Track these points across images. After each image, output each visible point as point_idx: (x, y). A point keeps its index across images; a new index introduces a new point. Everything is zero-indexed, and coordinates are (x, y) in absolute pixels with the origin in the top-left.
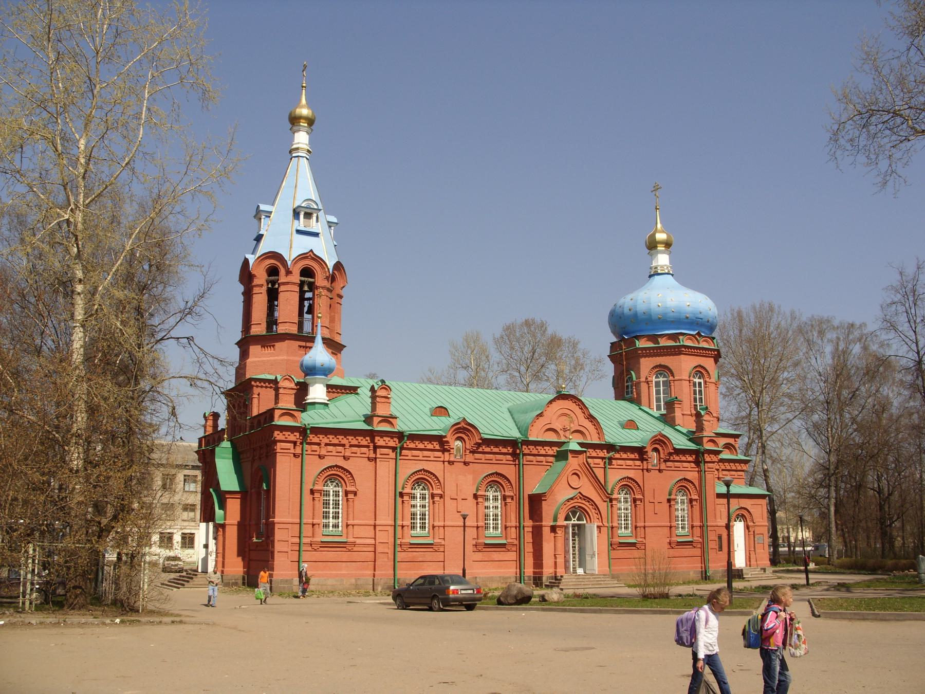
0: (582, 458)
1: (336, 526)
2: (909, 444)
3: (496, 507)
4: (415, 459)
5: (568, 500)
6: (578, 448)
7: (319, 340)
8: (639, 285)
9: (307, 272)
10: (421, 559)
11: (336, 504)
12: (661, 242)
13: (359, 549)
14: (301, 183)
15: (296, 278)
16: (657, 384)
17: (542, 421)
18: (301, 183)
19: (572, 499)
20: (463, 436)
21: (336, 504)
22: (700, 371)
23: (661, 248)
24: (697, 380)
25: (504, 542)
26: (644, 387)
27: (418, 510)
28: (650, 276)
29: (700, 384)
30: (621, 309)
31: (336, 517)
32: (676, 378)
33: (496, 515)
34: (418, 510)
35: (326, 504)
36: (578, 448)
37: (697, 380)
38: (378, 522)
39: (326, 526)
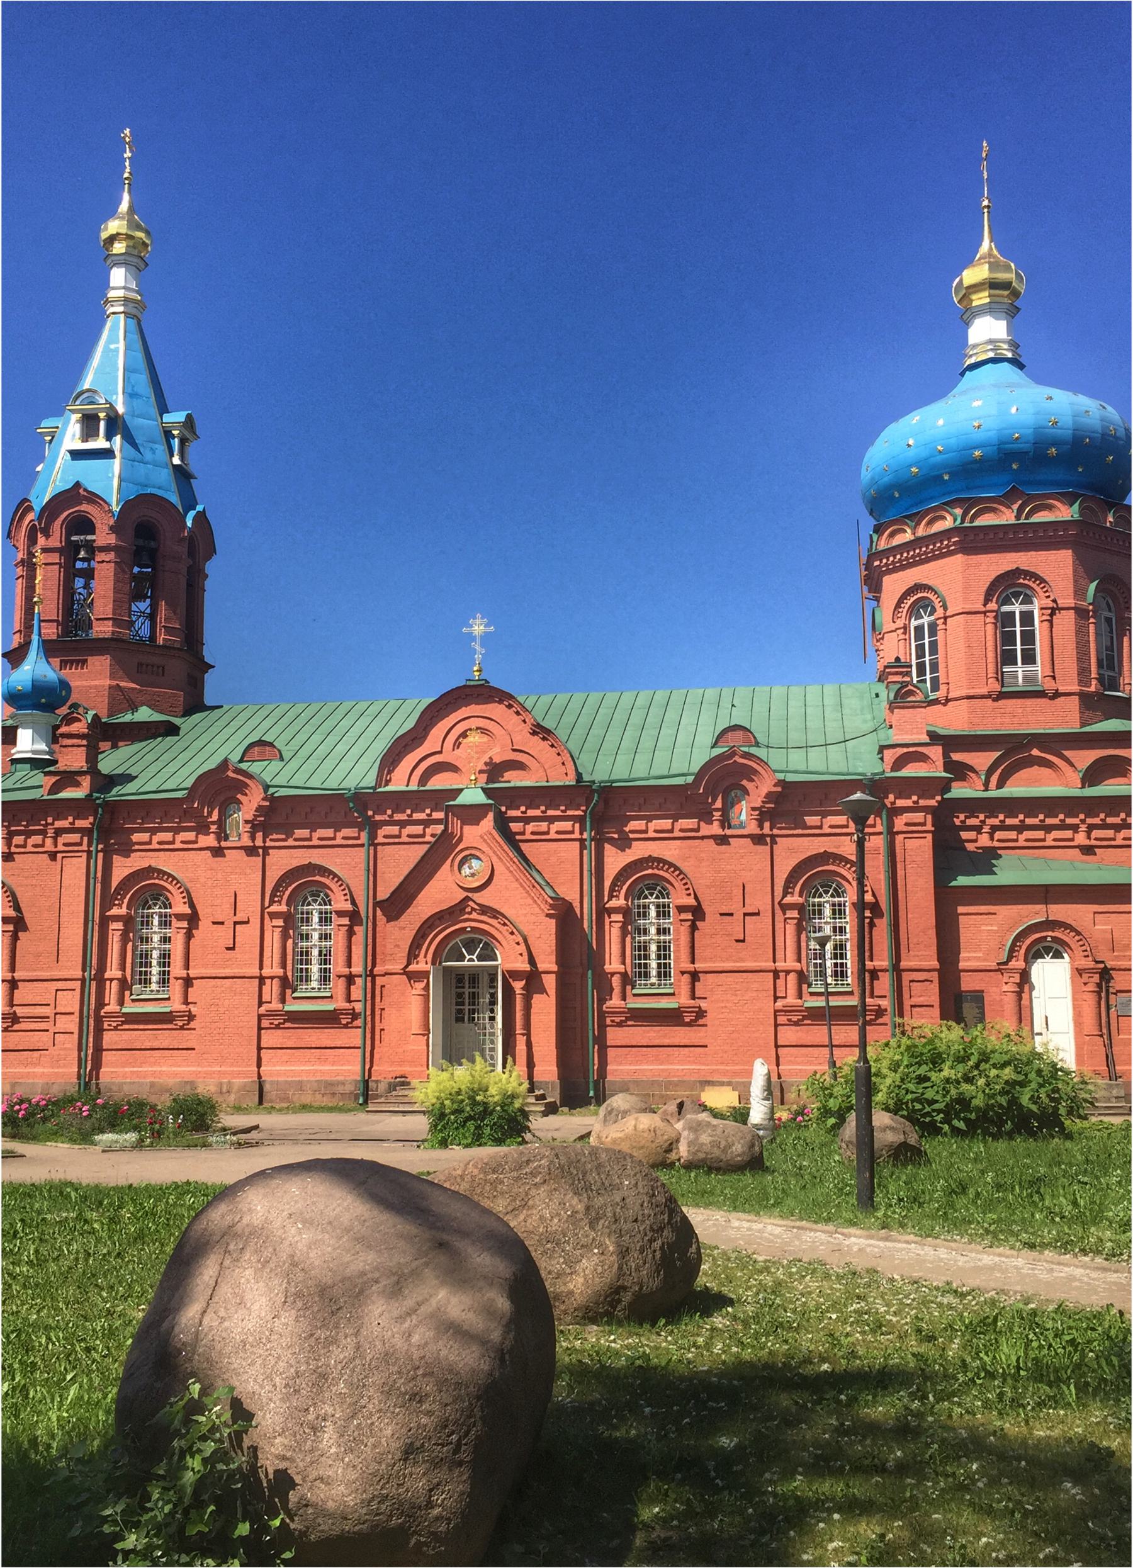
29: (1027, 618)
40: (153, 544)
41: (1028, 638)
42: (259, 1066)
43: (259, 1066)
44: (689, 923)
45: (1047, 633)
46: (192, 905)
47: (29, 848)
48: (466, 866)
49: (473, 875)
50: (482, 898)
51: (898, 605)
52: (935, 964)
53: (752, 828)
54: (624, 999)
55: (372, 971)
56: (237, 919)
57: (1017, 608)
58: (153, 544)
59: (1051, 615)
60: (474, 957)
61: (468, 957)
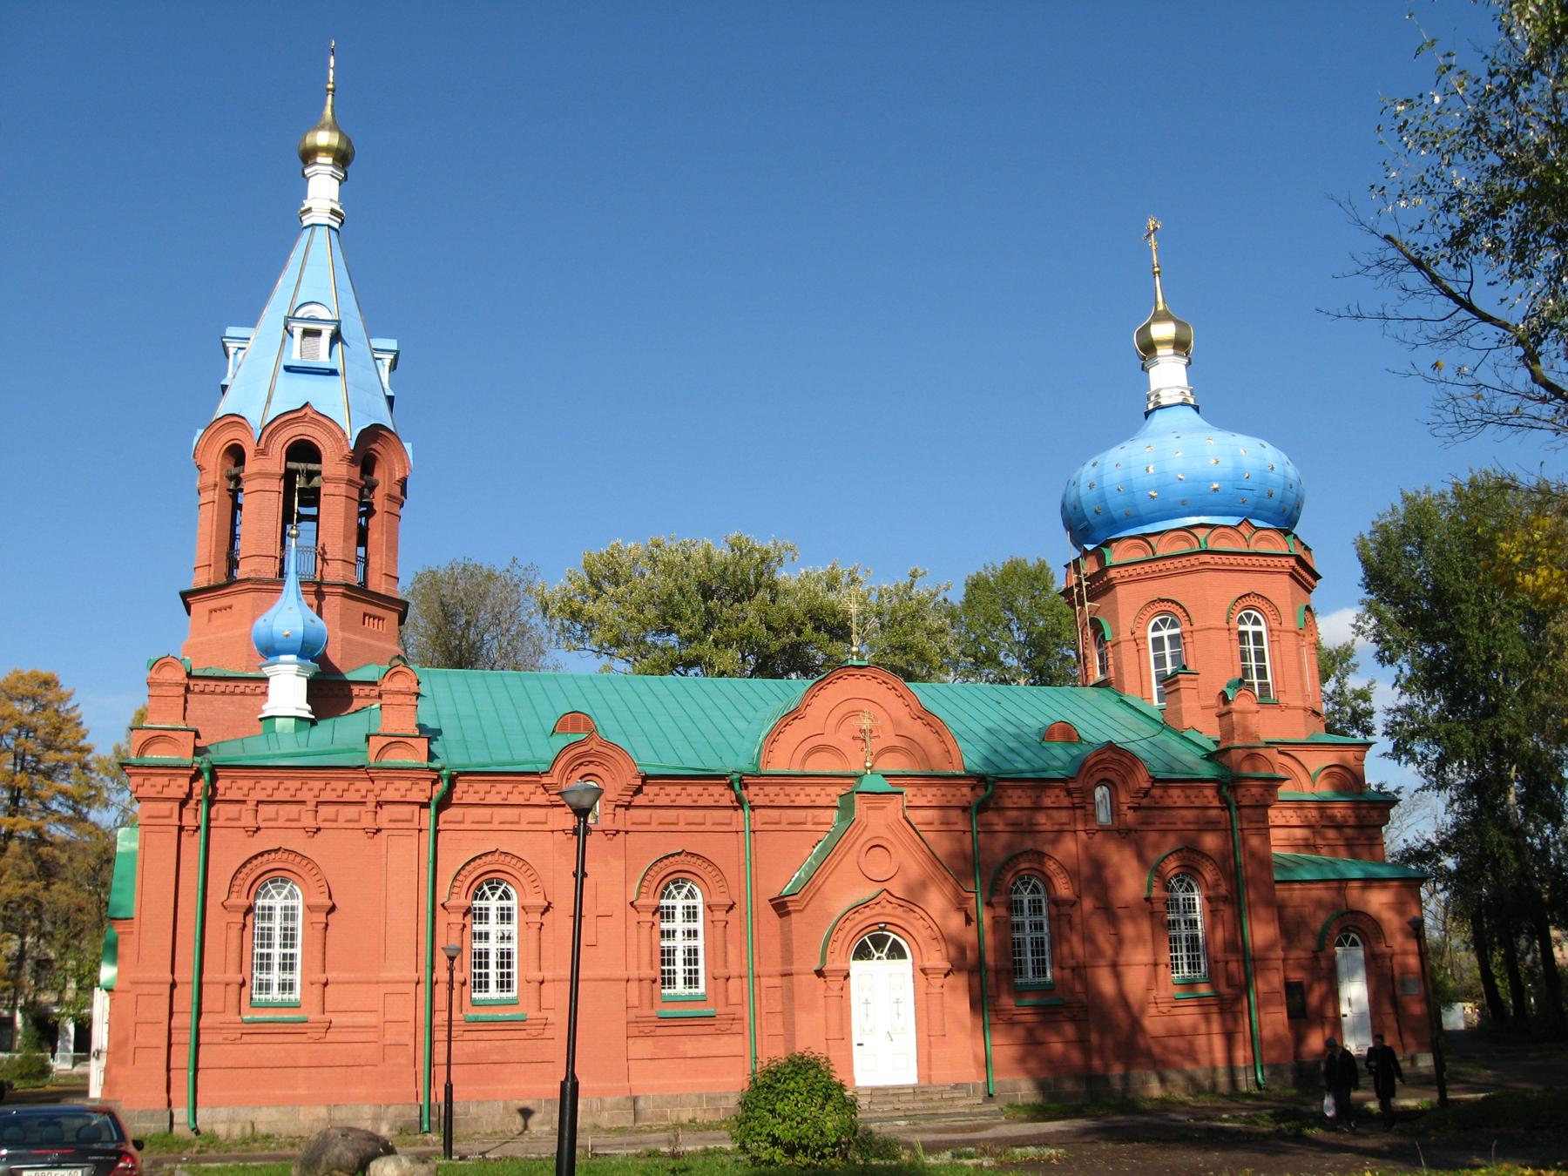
0: (894, 807)
1: (286, 986)
2: (643, 575)
3: (692, 934)
4: (483, 827)
5: (855, 909)
6: (885, 785)
7: (292, 581)
8: (1128, 432)
9: (304, 451)
10: (496, 1058)
11: (288, 938)
12: (1164, 343)
13: (340, 1038)
14: (315, 278)
15: (276, 462)
16: (1158, 643)
17: (796, 732)
18: (315, 278)
19: (865, 904)
20: (591, 769)
21: (288, 938)
22: (1249, 602)
23: (1164, 352)
24: (1249, 628)
25: (709, 1011)
26: (1127, 651)
27: (493, 946)
28: (1147, 414)
29: (1258, 637)
30: (1094, 492)
31: (287, 965)
32: (1196, 626)
33: (693, 952)
34: (493, 946)
35: (266, 936)
36: (885, 785)
37: (1249, 628)
38: (331, 975)
39: (265, 987)
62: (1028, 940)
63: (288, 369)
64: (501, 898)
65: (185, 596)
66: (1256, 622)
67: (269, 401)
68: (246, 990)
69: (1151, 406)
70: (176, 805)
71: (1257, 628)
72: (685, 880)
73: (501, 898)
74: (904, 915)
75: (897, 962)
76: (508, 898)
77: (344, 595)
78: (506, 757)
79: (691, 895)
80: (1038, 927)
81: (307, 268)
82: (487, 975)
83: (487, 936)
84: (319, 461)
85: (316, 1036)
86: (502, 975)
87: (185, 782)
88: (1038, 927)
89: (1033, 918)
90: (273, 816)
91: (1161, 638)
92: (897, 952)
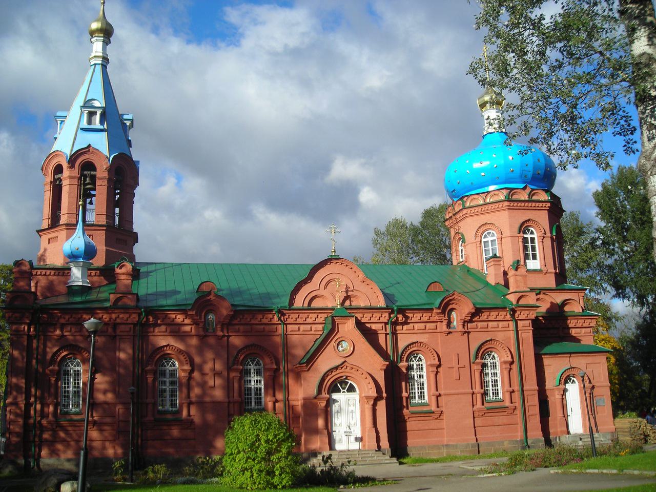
28: (483, 137)
29: (533, 240)
37: (529, 236)
38: (442, 392)
40: (93, 173)
41: (533, 248)
42: (476, 435)
43: (476, 435)
44: (238, 377)
45: (541, 247)
46: (439, 360)
47: (489, 329)
48: (340, 346)
49: (343, 350)
50: (350, 360)
51: (478, 230)
52: (537, 388)
53: (460, 328)
54: (483, 404)
55: (288, 399)
56: (459, 366)
57: (529, 236)
58: (93, 173)
59: (501, 240)
60: (345, 391)
61: (342, 391)
62: (168, 389)
63: (81, 129)
64: (418, 361)
65: (38, 231)
66: (532, 233)
67: (73, 144)
68: (474, 396)
69: (485, 133)
70: (383, 325)
71: (532, 236)
72: (491, 352)
73: (256, 365)
74: (341, 371)
75: (574, 384)
76: (174, 366)
77: (67, 229)
78: (415, 302)
79: (420, 359)
80: (421, 377)
81: (91, 84)
82: (251, 399)
83: (165, 382)
84: (95, 170)
85: (510, 412)
86: (172, 400)
87: (387, 315)
88: (421, 377)
89: (170, 379)
90: (128, 330)
91: (488, 242)
92: (351, 389)
